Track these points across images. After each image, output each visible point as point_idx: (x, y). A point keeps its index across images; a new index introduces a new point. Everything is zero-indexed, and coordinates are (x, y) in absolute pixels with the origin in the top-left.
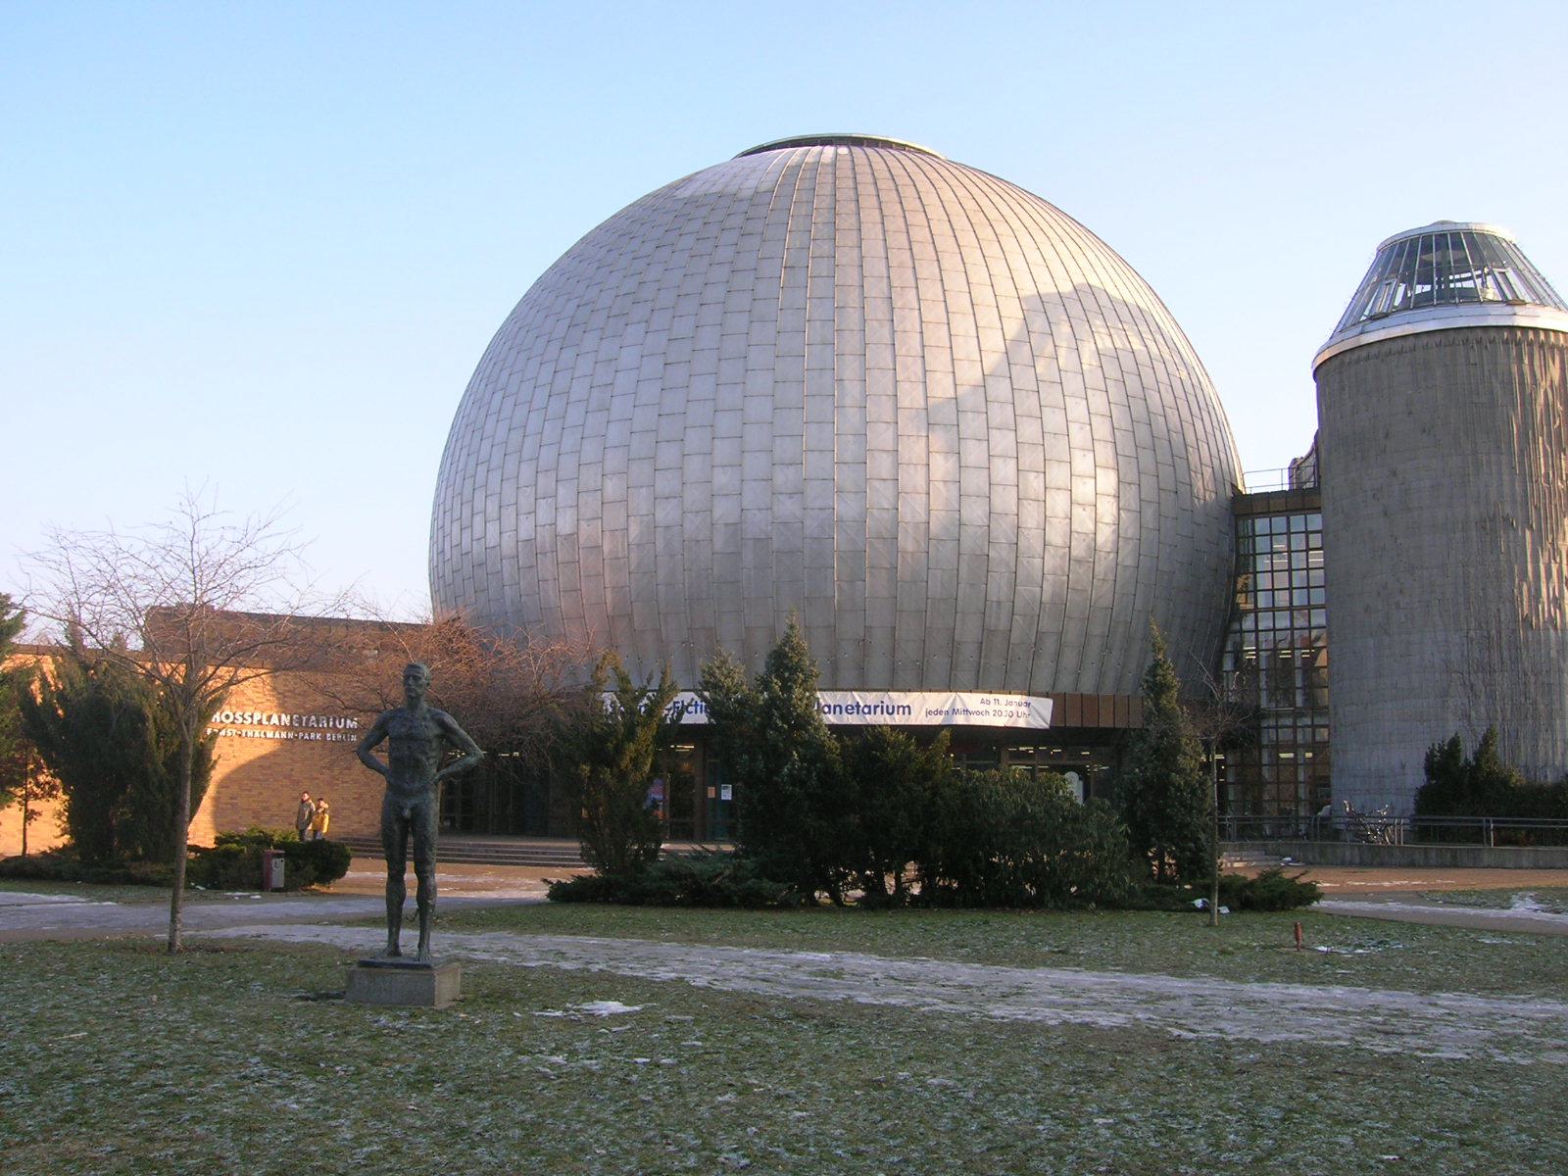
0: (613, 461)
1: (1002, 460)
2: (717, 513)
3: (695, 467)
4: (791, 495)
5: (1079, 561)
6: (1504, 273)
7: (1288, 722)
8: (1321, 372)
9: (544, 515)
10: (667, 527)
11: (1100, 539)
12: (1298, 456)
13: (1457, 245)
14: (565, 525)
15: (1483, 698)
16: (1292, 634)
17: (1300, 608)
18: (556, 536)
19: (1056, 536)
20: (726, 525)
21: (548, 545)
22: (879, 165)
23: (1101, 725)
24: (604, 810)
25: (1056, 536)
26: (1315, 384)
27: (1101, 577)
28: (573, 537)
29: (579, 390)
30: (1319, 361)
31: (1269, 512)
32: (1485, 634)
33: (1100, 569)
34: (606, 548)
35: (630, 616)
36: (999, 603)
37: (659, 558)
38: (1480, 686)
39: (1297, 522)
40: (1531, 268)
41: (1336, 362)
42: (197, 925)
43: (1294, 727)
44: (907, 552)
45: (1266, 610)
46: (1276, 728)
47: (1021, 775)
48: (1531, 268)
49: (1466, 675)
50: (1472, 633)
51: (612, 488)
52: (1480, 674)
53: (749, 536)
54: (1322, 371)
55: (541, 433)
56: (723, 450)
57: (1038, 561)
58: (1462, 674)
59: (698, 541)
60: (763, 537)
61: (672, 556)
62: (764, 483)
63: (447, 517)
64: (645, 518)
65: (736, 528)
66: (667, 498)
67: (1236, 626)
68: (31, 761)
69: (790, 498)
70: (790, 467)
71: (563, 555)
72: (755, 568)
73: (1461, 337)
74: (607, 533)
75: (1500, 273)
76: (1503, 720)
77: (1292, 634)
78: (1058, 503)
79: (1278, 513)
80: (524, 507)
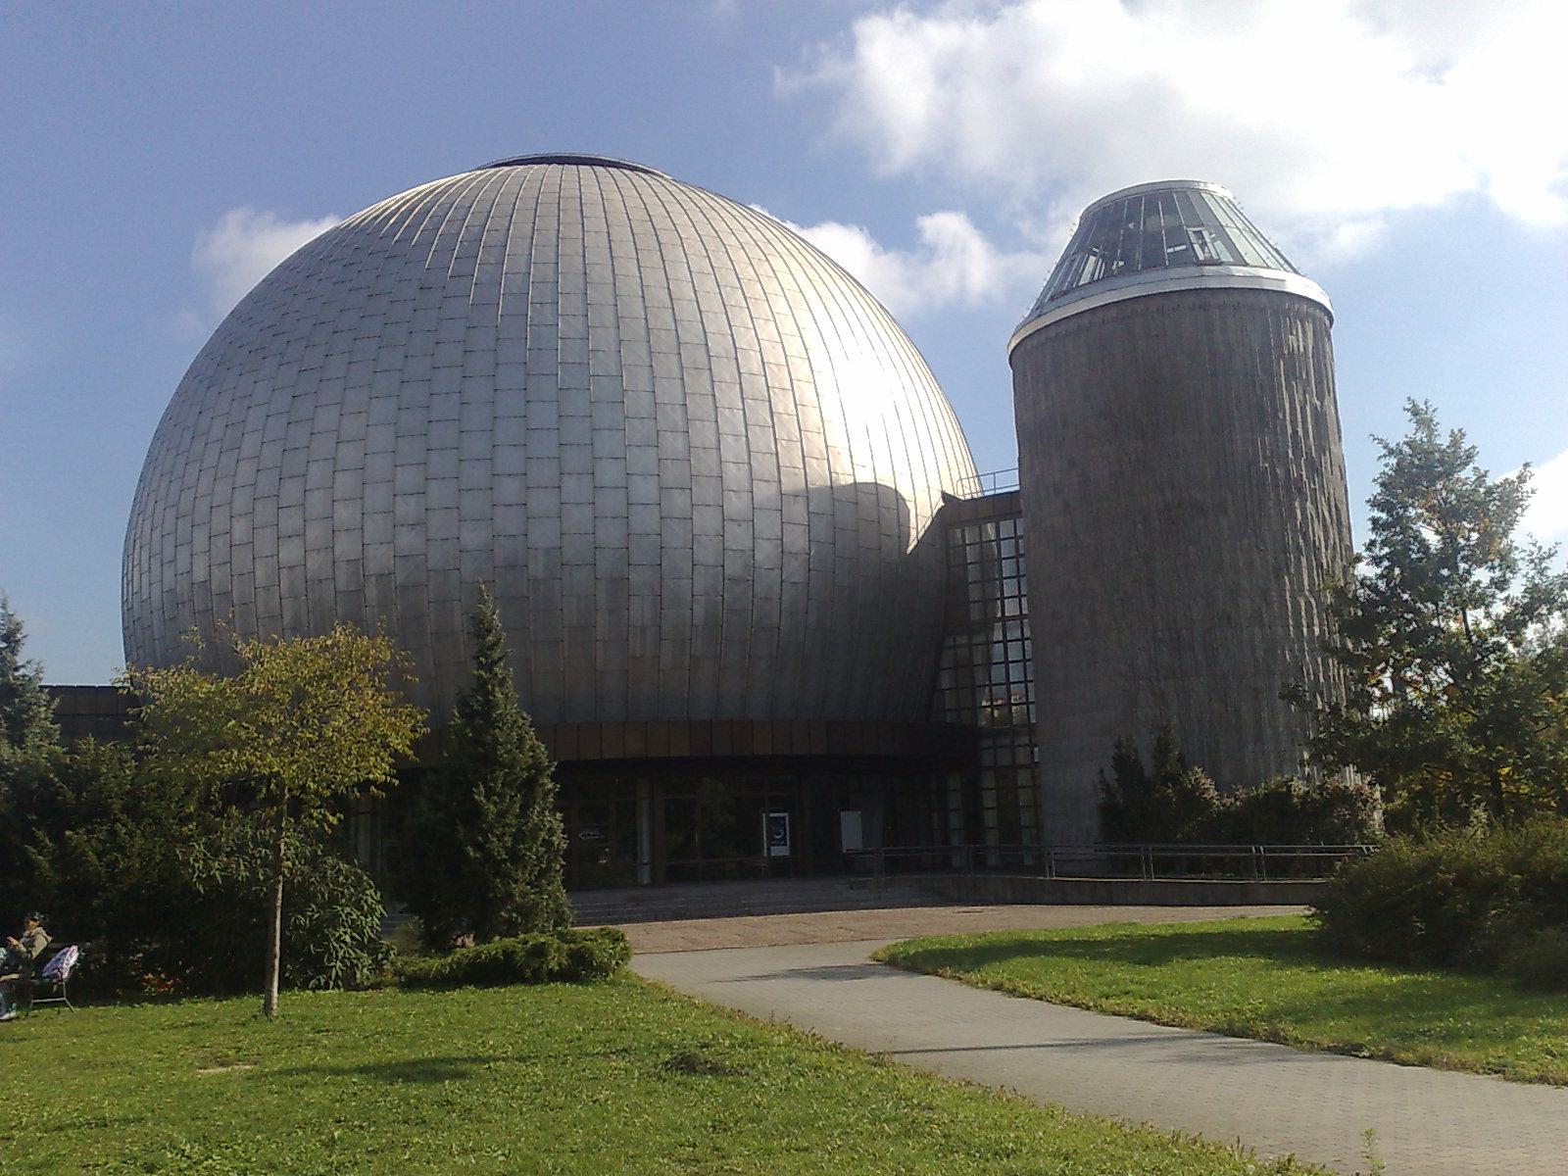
0: (241, 501)
1: (641, 478)
3: (316, 502)
5: (735, 581)
6: (1200, 232)
7: (1007, 741)
9: (182, 565)
11: (759, 556)
13: (1170, 210)
16: (1005, 636)
17: (1013, 618)
21: (186, 595)
22: (625, 184)
23: (607, 756)
24: (1442, 707)
28: (206, 584)
29: (217, 431)
30: (1013, 345)
36: (643, 628)
39: (1007, 527)
40: (1252, 229)
41: (1017, 352)
42: (1300, 765)
48: (1252, 229)
51: (240, 529)
56: (345, 483)
63: (147, 566)
65: (359, 563)
67: (950, 642)
69: (413, 529)
74: (285, 571)
75: (1195, 232)
77: (1005, 636)
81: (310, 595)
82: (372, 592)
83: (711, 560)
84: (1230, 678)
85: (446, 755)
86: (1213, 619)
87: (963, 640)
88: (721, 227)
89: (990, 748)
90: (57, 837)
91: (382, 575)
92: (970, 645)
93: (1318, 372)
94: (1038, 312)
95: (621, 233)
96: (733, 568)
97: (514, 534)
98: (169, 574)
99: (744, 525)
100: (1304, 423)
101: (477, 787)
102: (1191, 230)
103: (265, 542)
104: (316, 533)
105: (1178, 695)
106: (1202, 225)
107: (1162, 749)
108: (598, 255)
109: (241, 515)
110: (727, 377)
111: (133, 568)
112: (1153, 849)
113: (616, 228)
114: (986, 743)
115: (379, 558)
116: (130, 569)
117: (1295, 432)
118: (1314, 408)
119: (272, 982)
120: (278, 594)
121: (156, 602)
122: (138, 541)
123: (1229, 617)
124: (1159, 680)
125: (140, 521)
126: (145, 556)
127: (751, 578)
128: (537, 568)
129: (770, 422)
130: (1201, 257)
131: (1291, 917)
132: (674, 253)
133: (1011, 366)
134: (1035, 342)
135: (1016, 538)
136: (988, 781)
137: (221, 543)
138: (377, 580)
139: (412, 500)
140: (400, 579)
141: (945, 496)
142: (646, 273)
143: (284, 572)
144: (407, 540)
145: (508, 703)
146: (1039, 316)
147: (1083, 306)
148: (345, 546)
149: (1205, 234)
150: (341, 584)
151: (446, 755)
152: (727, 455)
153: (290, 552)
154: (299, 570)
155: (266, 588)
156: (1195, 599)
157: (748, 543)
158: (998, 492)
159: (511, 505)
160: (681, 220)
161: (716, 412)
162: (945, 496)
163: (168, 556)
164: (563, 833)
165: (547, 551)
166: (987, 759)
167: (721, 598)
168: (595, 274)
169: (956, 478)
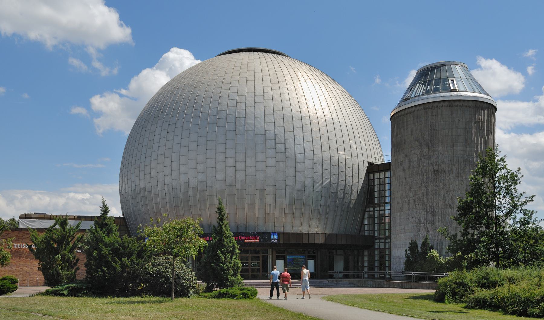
2: (181, 180)
3: (175, 165)
5: (298, 190)
7: (383, 241)
8: (393, 118)
10: (168, 184)
11: (306, 183)
12: (47, 214)
14: (142, 186)
15: (431, 232)
18: (140, 188)
19: (290, 182)
20: (184, 183)
21: (139, 192)
25: (290, 182)
26: (391, 122)
27: (307, 195)
28: (144, 188)
30: (392, 114)
31: (378, 171)
32: (433, 210)
33: (307, 193)
34: (153, 192)
37: (166, 194)
38: (430, 229)
43: (385, 243)
44: (239, 190)
45: (388, 203)
46: (379, 243)
47: (457, 268)
49: (426, 225)
50: (428, 210)
52: (430, 224)
53: (191, 186)
54: (393, 118)
55: (136, 156)
57: (284, 191)
58: (424, 224)
59: (176, 189)
60: (195, 186)
61: (170, 193)
62: (194, 169)
64: (162, 182)
65: (187, 183)
66: (168, 175)
67: (368, 210)
68: (138, 279)
70: (202, 164)
71: (142, 194)
72: (193, 196)
73: (430, 105)
75: (451, 80)
76: (438, 240)
78: (290, 171)
79: (381, 171)
80: (133, 180)
81: (174, 193)
82: (191, 193)
83: (291, 184)
84: (448, 224)
85: (212, 264)
86: (445, 206)
87: (372, 209)
88: (299, 74)
89: (378, 243)
90: (120, 260)
91: (194, 187)
92: (374, 211)
93: (488, 127)
94: (399, 105)
95: (266, 78)
96: (298, 187)
97: (232, 175)
98: (133, 185)
99: (302, 173)
100: (481, 144)
101: (218, 251)
102: (450, 80)
103: (161, 175)
104: (175, 174)
105: (432, 229)
106: (454, 77)
107: (425, 244)
108: (259, 86)
109: (153, 168)
110: (298, 126)
111: (123, 182)
112: (416, 273)
113: (265, 76)
114: (377, 241)
115: (193, 182)
116: (122, 183)
117: (477, 147)
118: (485, 138)
119: (173, 294)
120: (165, 192)
121: (130, 193)
122: (124, 175)
123: (450, 206)
124: (427, 224)
125: (124, 169)
126: (126, 180)
127: (304, 190)
128: (239, 186)
129: (312, 140)
130: (452, 88)
131: (432, 292)
132: (283, 84)
133: (391, 120)
134: (398, 115)
135: (390, 177)
136: (377, 252)
137: (148, 177)
138: (192, 189)
139: (202, 165)
140: (199, 188)
141: (369, 163)
142: (274, 91)
143: (166, 186)
144: (201, 177)
145: (228, 232)
146: (399, 107)
147: (413, 104)
148: (183, 178)
149: (455, 81)
150: (182, 190)
151: (212, 264)
152: (297, 151)
153: (168, 180)
154: (170, 185)
155: (161, 190)
156: (440, 199)
157: (303, 179)
158: (386, 162)
159: (231, 167)
160: (286, 72)
161: (294, 137)
162: (369, 163)
163: (133, 180)
164: (115, 223)
165: (242, 181)
166: (377, 246)
167: (294, 196)
168: (258, 92)
169: (373, 156)
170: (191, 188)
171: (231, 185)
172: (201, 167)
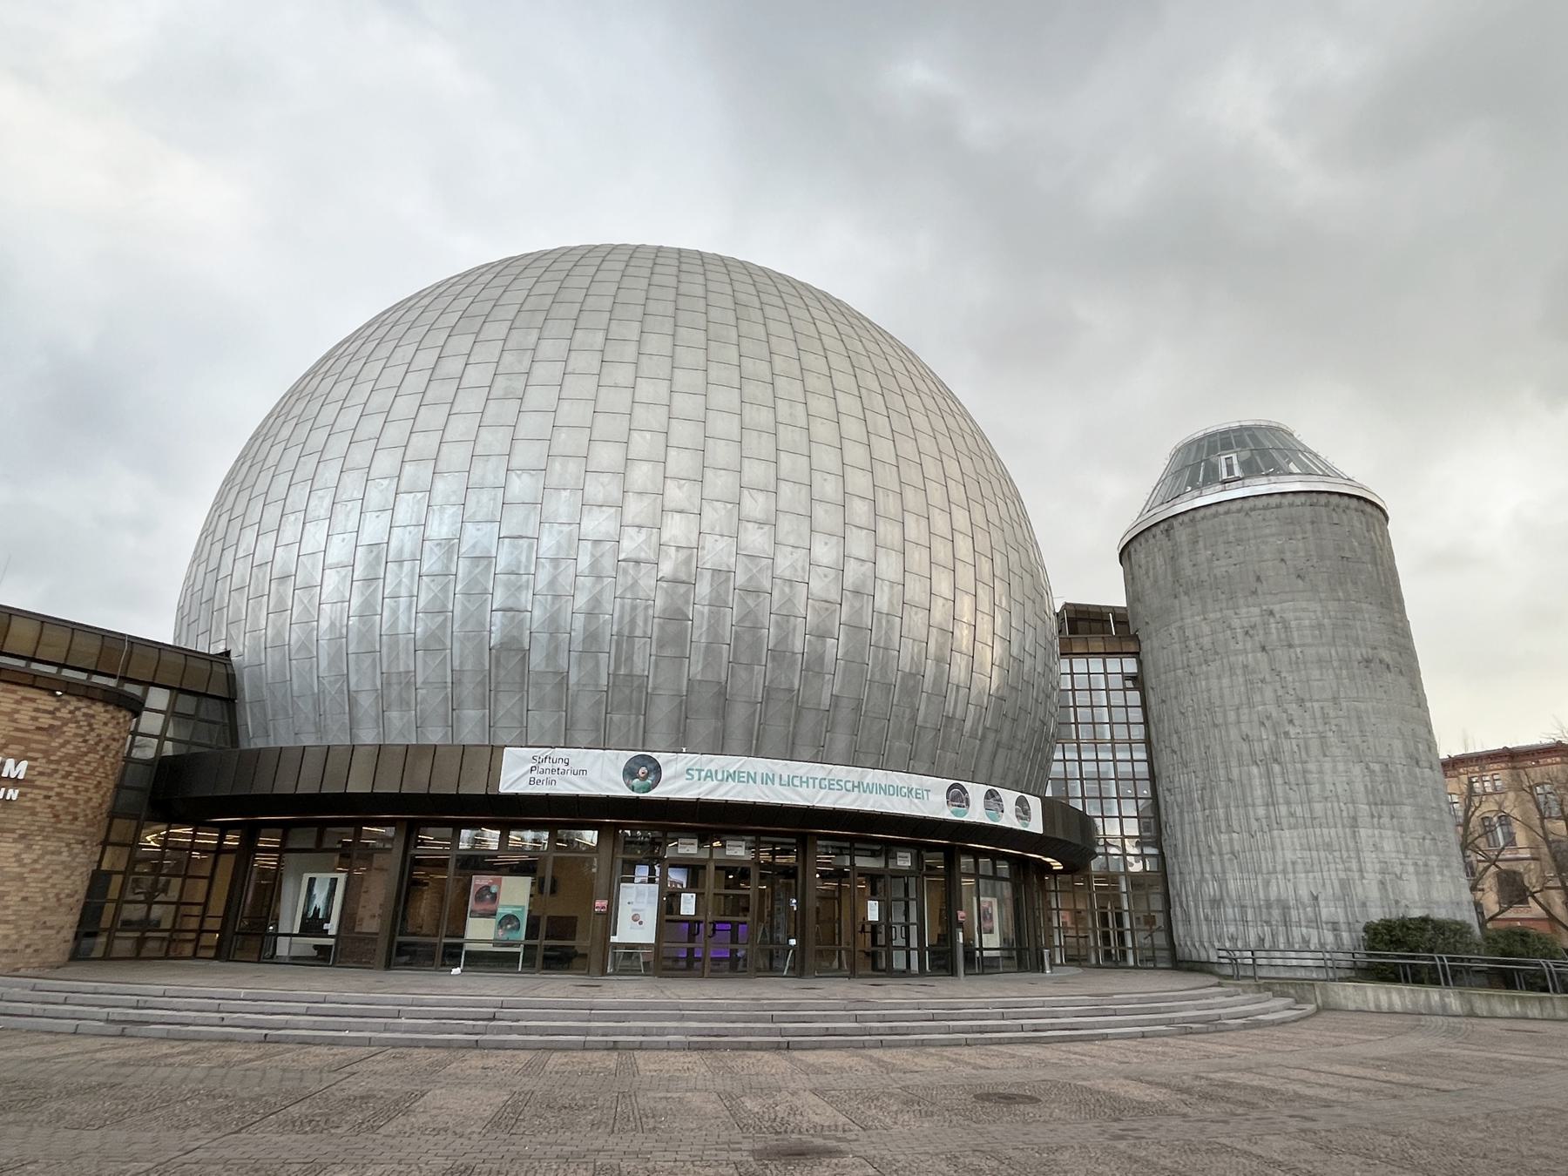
4: (761, 524)
35: (525, 655)
82: (704, 589)
115: (717, 551)
144: (755, 539)
148: (677, 529)
170: (708, 575)
171: (857, 593)
172: (755, 505)
